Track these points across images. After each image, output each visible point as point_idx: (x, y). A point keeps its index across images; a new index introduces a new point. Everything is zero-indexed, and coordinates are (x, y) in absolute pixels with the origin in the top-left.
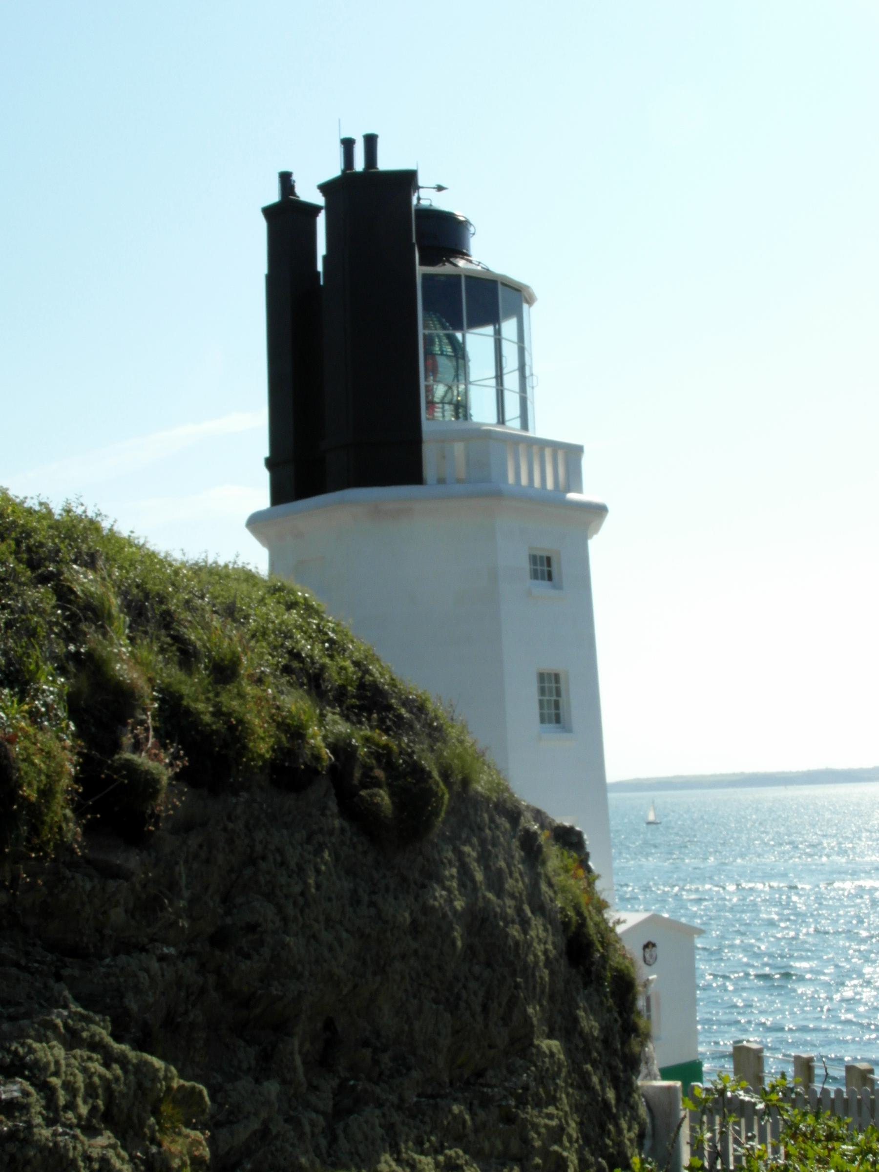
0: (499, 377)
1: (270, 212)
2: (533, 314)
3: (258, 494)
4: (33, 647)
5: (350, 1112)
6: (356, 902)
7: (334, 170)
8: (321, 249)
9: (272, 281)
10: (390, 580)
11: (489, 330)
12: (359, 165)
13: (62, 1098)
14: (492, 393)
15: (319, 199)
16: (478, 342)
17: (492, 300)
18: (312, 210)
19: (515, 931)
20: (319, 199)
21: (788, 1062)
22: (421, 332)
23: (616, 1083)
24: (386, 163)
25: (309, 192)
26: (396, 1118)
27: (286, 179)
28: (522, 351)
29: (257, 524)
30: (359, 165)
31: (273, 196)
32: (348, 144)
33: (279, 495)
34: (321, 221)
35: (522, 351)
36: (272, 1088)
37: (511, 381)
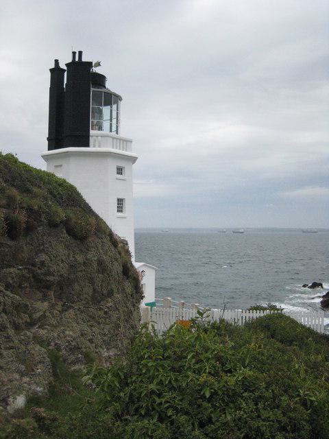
0: (111, 120)
1: (51, 70)
2: (122, 104)
5: (66, 311)
7: (70, 60)
8: (65, 82)
9: (51, 89)
11: (109, 107)
12: (77, 59)
15: (66, 68)
16: (106, 110)
19: (110, 266)
20: (66, 68)
22: (91, 120)
23: (134, 306)
24: (84, 59)
25: (63, 66)
26: (78, 312)
27: (57, 62)
28: (117, 127)
30: (77, 59)
31: (53, 66)
32: (74, 53)
34: (66, 73)
35: (117, 127)
36: (46, 304)
37: (114, 121)
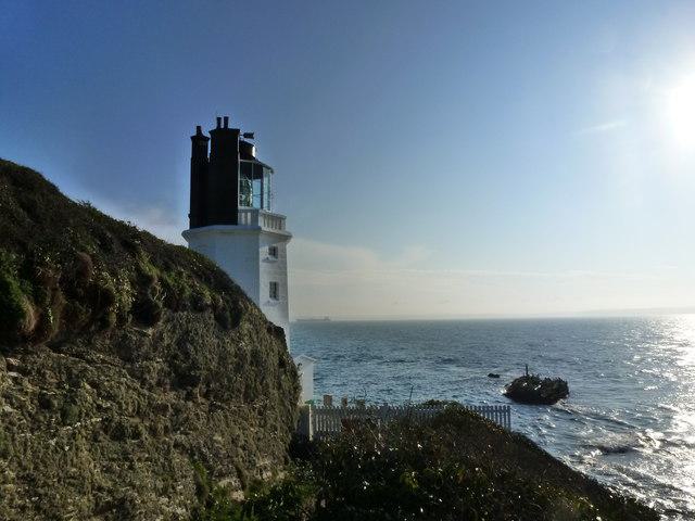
0: (262, 195)
3: (186, 224)
4: (648, 349)
6: (219, 346)
7: (214, 127)
8: (209, 152)
10: (221, 249)
13: (124, 406)
14: (259, 200)
16: (256, 184)
17: (257, 171)
18: (206, 139)
20: (209, 136)
21: (219, 123)
27: (199, 128)
29: (185, 234)
32: (219, 119)
33: (192, 226)
37: (265, 196)
